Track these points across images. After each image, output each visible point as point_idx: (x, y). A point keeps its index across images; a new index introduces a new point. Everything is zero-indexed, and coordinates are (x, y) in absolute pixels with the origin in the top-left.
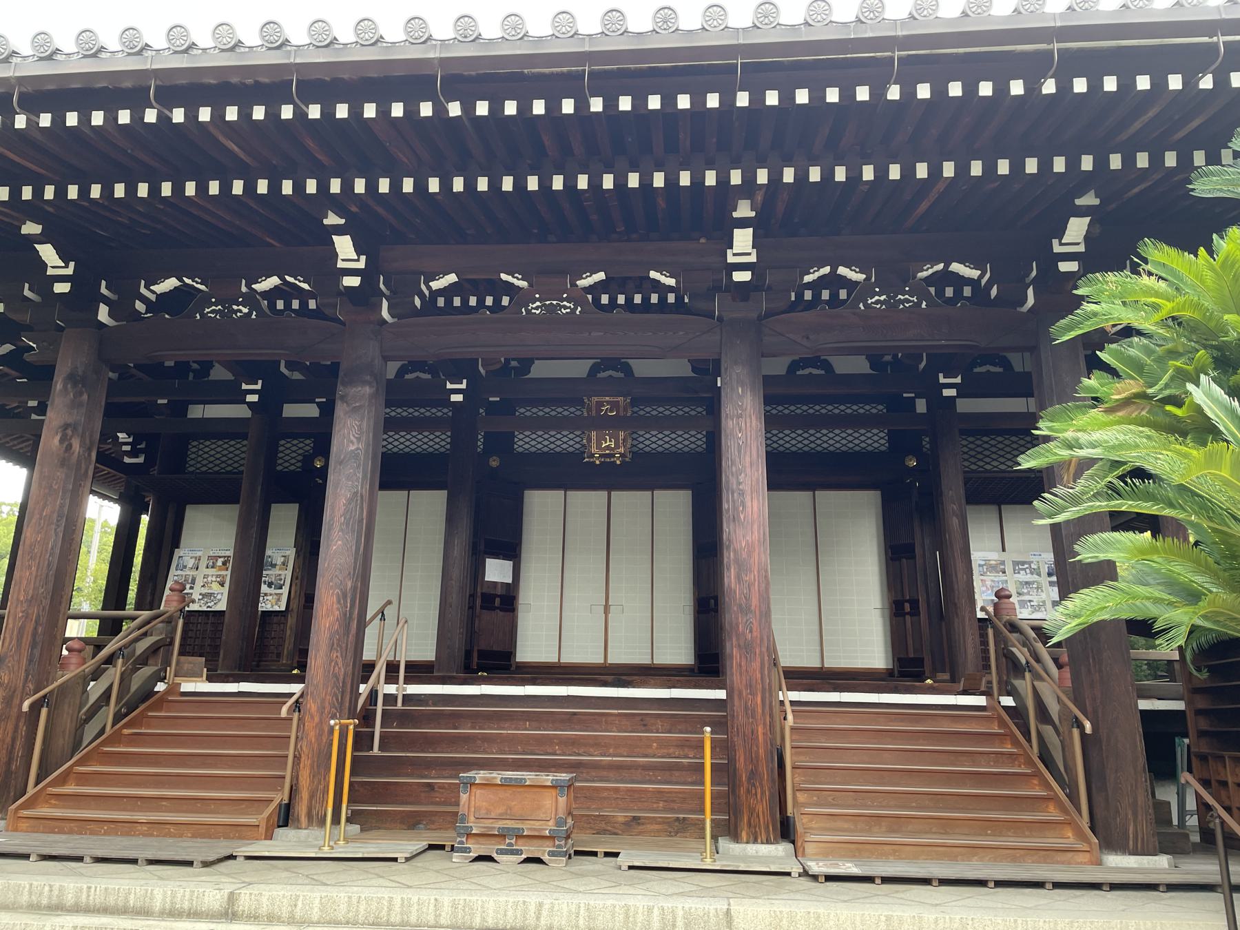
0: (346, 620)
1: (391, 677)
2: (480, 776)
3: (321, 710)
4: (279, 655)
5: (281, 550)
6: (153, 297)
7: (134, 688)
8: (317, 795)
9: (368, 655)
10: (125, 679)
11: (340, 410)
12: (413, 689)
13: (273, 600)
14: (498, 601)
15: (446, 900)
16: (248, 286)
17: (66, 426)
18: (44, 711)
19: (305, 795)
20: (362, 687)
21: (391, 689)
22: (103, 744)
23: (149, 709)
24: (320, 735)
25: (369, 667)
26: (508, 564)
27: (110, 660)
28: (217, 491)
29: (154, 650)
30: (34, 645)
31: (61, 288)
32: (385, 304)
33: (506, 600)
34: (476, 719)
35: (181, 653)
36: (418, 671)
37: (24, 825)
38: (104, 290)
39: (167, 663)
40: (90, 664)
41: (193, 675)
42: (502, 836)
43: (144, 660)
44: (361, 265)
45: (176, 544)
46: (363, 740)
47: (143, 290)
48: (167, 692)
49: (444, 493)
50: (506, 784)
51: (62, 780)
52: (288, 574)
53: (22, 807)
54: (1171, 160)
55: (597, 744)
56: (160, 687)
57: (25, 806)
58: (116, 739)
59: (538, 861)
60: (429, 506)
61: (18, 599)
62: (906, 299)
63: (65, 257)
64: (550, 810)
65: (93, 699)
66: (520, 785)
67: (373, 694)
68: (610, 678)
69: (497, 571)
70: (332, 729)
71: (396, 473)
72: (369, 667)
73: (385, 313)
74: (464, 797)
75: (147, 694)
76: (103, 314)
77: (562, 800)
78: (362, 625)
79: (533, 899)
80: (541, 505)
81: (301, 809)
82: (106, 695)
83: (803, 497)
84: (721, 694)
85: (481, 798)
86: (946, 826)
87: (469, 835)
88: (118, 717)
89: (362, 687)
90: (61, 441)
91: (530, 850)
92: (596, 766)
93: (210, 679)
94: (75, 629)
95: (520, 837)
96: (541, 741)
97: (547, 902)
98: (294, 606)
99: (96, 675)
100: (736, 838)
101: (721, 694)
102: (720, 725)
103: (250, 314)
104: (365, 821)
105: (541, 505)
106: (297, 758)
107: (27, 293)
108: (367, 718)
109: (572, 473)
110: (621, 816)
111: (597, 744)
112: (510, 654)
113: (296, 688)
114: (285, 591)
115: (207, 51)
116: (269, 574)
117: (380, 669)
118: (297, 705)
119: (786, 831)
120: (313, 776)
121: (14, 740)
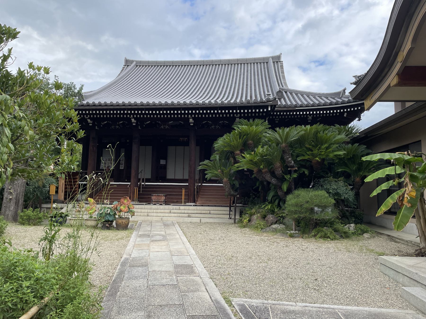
9: (139, 177)
12: (146, 184)
13: (122, 167)
21: (143, 183)
33: (165, 167)
36: (148, 180)
41: (112, 181)
42: (157, 201)
49: (151, 147)
50: (157, 195)
60: (149, 149)
62: (217, 127)
64: (163, 198)
67: (140, 184)
69: (162, 162)
71: (143, 142)
73: (139, 128)
76: (96, 128)
78: (138, 174)
80: (171, 149)
84: (187, 184)
85: (153, 198)
101: (187, 184)
105: (171, 149)
109: (177, 143)
110: (175, 201)
113: (129, 183)
114: (123, 165)
117: (141, 180)
118: (130, 186)
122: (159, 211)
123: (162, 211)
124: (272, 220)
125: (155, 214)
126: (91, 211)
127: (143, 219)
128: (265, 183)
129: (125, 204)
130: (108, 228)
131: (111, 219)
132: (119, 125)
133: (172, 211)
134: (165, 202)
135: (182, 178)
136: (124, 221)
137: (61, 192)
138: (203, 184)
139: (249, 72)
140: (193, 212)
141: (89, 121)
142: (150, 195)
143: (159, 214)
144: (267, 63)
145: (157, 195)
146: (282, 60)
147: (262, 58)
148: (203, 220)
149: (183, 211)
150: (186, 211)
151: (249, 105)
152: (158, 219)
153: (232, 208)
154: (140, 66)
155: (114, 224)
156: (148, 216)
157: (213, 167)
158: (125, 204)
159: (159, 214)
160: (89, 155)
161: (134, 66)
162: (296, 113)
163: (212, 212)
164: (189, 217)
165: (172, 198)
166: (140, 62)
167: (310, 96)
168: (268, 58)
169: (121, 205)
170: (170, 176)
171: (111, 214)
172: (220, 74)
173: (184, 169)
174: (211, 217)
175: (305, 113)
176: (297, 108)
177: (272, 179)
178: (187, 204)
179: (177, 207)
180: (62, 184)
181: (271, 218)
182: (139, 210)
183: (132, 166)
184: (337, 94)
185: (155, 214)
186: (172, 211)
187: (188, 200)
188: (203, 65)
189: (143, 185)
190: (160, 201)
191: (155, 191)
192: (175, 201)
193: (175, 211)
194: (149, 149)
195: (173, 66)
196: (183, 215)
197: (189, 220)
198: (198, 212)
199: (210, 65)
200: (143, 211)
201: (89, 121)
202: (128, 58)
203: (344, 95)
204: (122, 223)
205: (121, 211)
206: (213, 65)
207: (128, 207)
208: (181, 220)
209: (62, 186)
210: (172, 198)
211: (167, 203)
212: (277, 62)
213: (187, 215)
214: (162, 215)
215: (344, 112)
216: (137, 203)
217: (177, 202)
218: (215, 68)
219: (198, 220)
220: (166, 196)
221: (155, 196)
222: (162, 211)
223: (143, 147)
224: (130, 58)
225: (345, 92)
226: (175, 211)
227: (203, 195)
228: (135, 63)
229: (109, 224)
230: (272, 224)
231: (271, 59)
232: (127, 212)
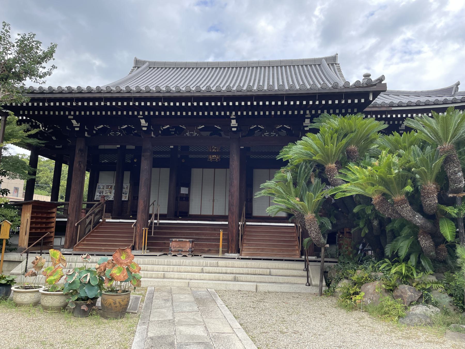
0: (145, 206)
1: (156, 219)
2: (174, 240)
3: (140, 226)
4: (126, 212)
5: (127, 185)
6: (97, 129)
7: (95, 221)
8: (140, 243)
9: (151, 212)
11: (143, 158)
12: (161, 221)
13: (125, 198)
14: (184, 199)
15: (166, 260)
16: (120, 127)
17: (80, 162)
18: (79, 226)
19: (137, 244)
20: (149, 221)
21: (156, 221)
22: (91, 233)
23: (99, 225)
24: (140, 231)
25: (150, 216)
26: (187, 189)
28: (108, 168)
29: (99, 212)
30: (76, 212)
31: (77, 129)
32: (152, 133)
33: (187, 198)
34: (198, 229)
35: (106, 212)
36: (163, 217)
37: (77, 250)
38: (86, 128)
39: (102, 215)
41: (108, 218)
42: (178, 251)
43: (96, 215)
44: (79, 125)
45: (97, 182)
46: (150, 233)
47: (95, 128)
50: (179, 241)
51: (83, 241)
52: (128, 190)
53: (76, 246)
54: (302, 112)
55: (203, 234)
56: (101, 220)
57: (76, 246)
58: (93, 232)
59: (186, 256)
60: (165, 172)
63: (78, 122)
64: (188, 246)
65: (87, 223)
66: (182, 241)
67: (152, 222)
68: (210, 219)
69: (184, 191)
70: (143, 230)
71: (157, 163)
72: (150, 216)
73: (153, 135)
74: (171, 244)
75: (98, 222)
76: (86, 134)
77: (191, 244)
78: (149, 206)
79: (182, 261)
80: (196, 173)
81: (137, 246)
82: (90, 223)
83: (268, 170)
84: (227, 223)
85: (173, 245)
86: (273, 250)
87: (172, 251)
89: (149, 221)
90: (79, 165)
91: (184, 254)
92: (203, 239)
93: (113, 219)
95: (182, 251)
96: (191, 233)
97: (184, 261)
98: (130, 199)
100: (228, 253)
101: (227, 223)
102: (224, 230)
103: (275, 135)
104: (151, 250)
105: (196, 173)
106: (135, 236)
107: (67, 128)
108: (150, 228)
109: (204, 164)
110: (206, 249)
111: (203, 234)
112: (188, 212)
113: (135, 221)
114: (127, 195)
116: (124, 190)
117: (153, 216)
119: (238, 251)
120: (139, 240)
121: (73, 232)
123: (189, 268)
124: (411, 296)
125: (176, 275)
126: (52, 278)
127: (156, 284)
128: (375, 223)
129: (121, 264)
130: (85, 314)
131: (91, 295)
132: (120, 131)
133: (207, 269)
134: (192, 252)
135: (223, 214)
136: (118, 299)
137: (24, 234)
138: (248, 223)
139: (298, 74)
140: (241, 270)
142: (168, 239)
143: (184, 275)
144: (319, 65)
145: (179, 241)
146: (338, 63)
147: (313, 59)
148: (263, 287)
149: (224, 270)
150: (229, 270)
151: (337, 91)
152: (181, 283)
154: (154, 68)
155: (99, 303)
156: (164, 278)
157: (274, 195)
158: (121, 264)
159: (184, 275)
160: (73, 175)
161: (146, 67)
163: (273, 271)
164: (235, 280)
165: (201, 245)
166: (155, 63)
168: (320, 60)
169: (114, 266)
170: (194, 211)
171: (93, 283)
172: (260, 77)
173: (213, 201)
174: (273, 281)
176: (393, 109)
177: (414, 216)
178: (227, 255)
179: (213, 261)
180: (26, 221)
181: (407, 291)
182: (149, 267)
183: (140, 198)
184: (447, 91)
185: (176, 275)
186: (207, 269)
187: (227, 249)
188: (237, 68)
189: (155, 224)
190: (183, 250)
191: (173, 233)
192: (206, 249)
193: (211, 269)
194: (165, 172)
195: (197, 68)
196: (225, 276)
197: (237, 286)
198: (250, 271)
199: (245, 68)
200: (156, 267)
202: (139, 58)
203: (456, 92)
204: (115, 303)
205: (112, 279)
206: (249, 68)
207: (128, 269)
208: (222, 286)
209: (25, 224)
210: (201, 245)
211: (194, 253)
212: (332, 64)
213: (231, 277)
214: (189, 275)
216: (146, 254)
217: (209, 251)
218: (252, 71)
219: (250, 287)
220: (193, 242)
221: (176, 241)
222: (189, 268)
223: (157, 169)
224: (140, 58)
225: (458, 88)
226: (211, 269)
227: (249, 240)
228: (147, 63)
229: (88, 305)
230: (410, 305)
231: (324, 61)
232: (125, 281)
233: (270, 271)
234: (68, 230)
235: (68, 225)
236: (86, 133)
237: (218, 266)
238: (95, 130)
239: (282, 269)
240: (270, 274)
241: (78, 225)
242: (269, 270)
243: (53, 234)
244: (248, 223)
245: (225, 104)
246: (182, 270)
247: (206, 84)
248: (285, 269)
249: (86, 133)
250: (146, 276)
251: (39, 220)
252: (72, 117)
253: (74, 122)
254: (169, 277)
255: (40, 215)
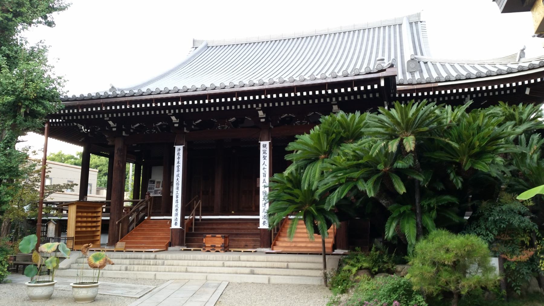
2: (207, 236)
10: (137, 216)
12: (203, 217)
27: (134, 212)
29: (144, 209)
40: (130, 213)
44: (178, 121)
48: (147, 219)
56: (146, 218)
61: (138, 208)
63: (177, 118)
65: (131, 221)
74: (204, 239)
79: (206, 256)
82: (133, 220)
88: (136, 225)
94: (125, 204)
99: (131, 215)
115: (83, 99)
122: (205, 263)
125: (198, 269)
133: (227, 263)
134: (225, 247)
140: (259, 264)
141: (174, 118)
142: (202, 234)
148: (275, 280)
149: (244, 264)
150: (248, 264)
153: (327, 257)
162: (440, 92)
164: (252, 273)
167: (466, 66)
175: (362, 88)
178: (259, 250)
186: (227, 263)
198: (268, 264)
200: (181, 262)
201: (174, 118)
211: (226, 248)
215: (524, 86)
219: (263, 279)
233: (287, 265)
234: (110, 228)
235: (111, 224)
236: (185, 128)
237: (240, 260)
238: (132, 129)
239: (302, 262)
240: (287, 268)
241: (119, 223)
242: (222, 262)
243: (99, 233)
244: (152, 218)
245: (356, 89)
246: (205, 265)
247: (320, 71)
248: (304, 262)
249: (185, 128)
250: (170, 270)
251: (85, 219)
252: (108, 119)
253: (111, 123)
254: (191, 270)
255: (85, 214)
